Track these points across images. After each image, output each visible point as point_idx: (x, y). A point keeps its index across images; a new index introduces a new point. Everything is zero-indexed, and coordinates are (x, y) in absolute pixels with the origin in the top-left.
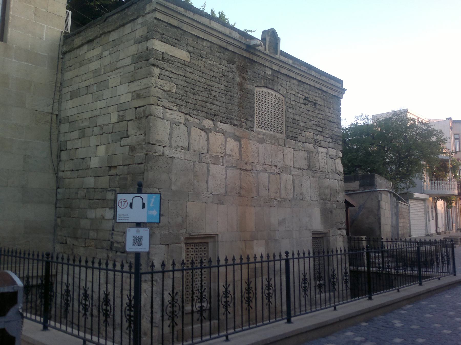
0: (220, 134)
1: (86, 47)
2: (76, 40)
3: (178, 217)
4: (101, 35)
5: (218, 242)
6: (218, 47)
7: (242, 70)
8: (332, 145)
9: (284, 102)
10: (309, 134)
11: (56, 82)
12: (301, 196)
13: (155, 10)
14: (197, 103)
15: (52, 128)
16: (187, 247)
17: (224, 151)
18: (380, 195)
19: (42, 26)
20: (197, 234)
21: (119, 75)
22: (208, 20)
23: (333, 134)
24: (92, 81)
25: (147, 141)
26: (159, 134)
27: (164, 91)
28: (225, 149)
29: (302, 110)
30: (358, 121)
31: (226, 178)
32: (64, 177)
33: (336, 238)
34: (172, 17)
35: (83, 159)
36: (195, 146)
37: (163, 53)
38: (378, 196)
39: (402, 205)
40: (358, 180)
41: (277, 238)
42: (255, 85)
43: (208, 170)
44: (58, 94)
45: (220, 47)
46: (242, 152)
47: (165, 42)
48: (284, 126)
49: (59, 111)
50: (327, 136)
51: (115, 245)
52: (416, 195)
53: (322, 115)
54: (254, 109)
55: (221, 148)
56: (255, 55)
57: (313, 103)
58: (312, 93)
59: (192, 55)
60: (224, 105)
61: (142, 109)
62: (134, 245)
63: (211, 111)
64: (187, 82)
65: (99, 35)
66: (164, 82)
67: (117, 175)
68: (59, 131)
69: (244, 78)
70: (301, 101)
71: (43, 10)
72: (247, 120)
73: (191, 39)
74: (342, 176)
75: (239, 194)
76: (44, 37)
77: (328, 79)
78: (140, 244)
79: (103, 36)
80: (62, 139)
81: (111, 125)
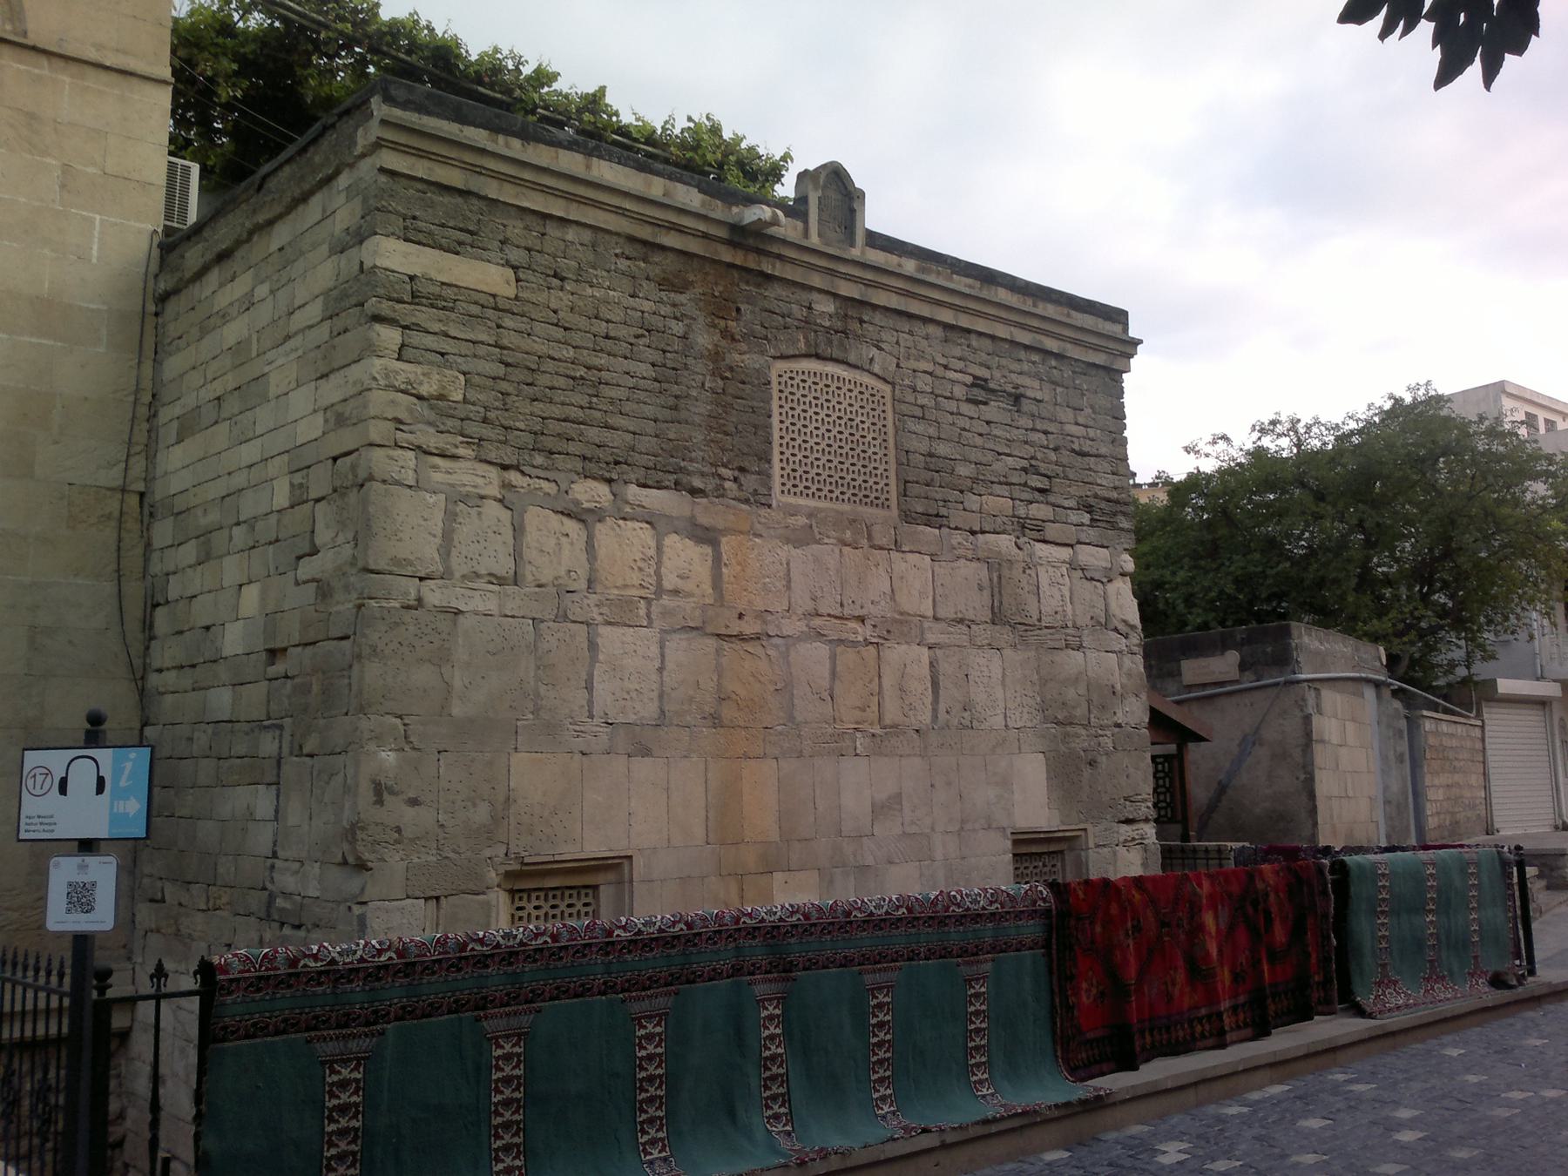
0: (637, 525)
1: (213, 277)
2: (187, 255)
3: (475, 805)
4: (251, 233)
5: (631, 881)
6: (621, 241)
7: (721, 309)
8: (1092, 534)
9: (888, 399)
10: (998, 502)
11: (137, 391)
12: (966, 714)
13: (379, 144)
14: (538, 429)
15: (124, 534)
16: (518, 904)
17: (653, 580)
18: (1311, 697)
19: (85, 219)
20: (550, 858)
21: (293, 356)
22: (579, 157)
23: (1096, 496)
24: (230, 381)
25: (360, 564)
26: (400, 540)
27: (420, 398)
28: (658, 574)
29: (962, 422)
30: (1266, 442)
31: (661, 670)
32: (162, 689)
33: (1115, 853)
34: (444, 161)
35: (207, 628)
36: (542, 567)
37: (412, 278)
38: (1304, 700)
39: (1438, 728)
40: (1236, 646)
41: (870, 861)
42: (772, 352)
43: (593, 646)
44: (145, 426)
45: (632, 239)
46: (725, 578)
47: (419, 243)
48: (893, 481)
49: (149, 479)
50: (1072, 503)
51: (280, 902)
52: (1505, 686)
53: (1046, 433)
54: (770, 434)
55: (640, 569)
56: (769, 254)
57: (1010, 395)
58: (1004, 362)
59: (522, 276)
60: (650, 427)
61: (348, 459)
62: (68, 911)
63: (600, 453)
64: (507, 365)
65: (245, 235)
66: (419, 369)
67: (287, 677)
68: (148, 545)
69: (726, 334)
70: (959, 391)
71: (90, 170)
72: (742, 470)
73: (520, 224)
74: (1136, 639)
75: (715, 720)
76: (95, 253)
77: (1065, 311)
78: (88, 908)
79: (255, 238)
80: (156, 568)
81: (273, 518)
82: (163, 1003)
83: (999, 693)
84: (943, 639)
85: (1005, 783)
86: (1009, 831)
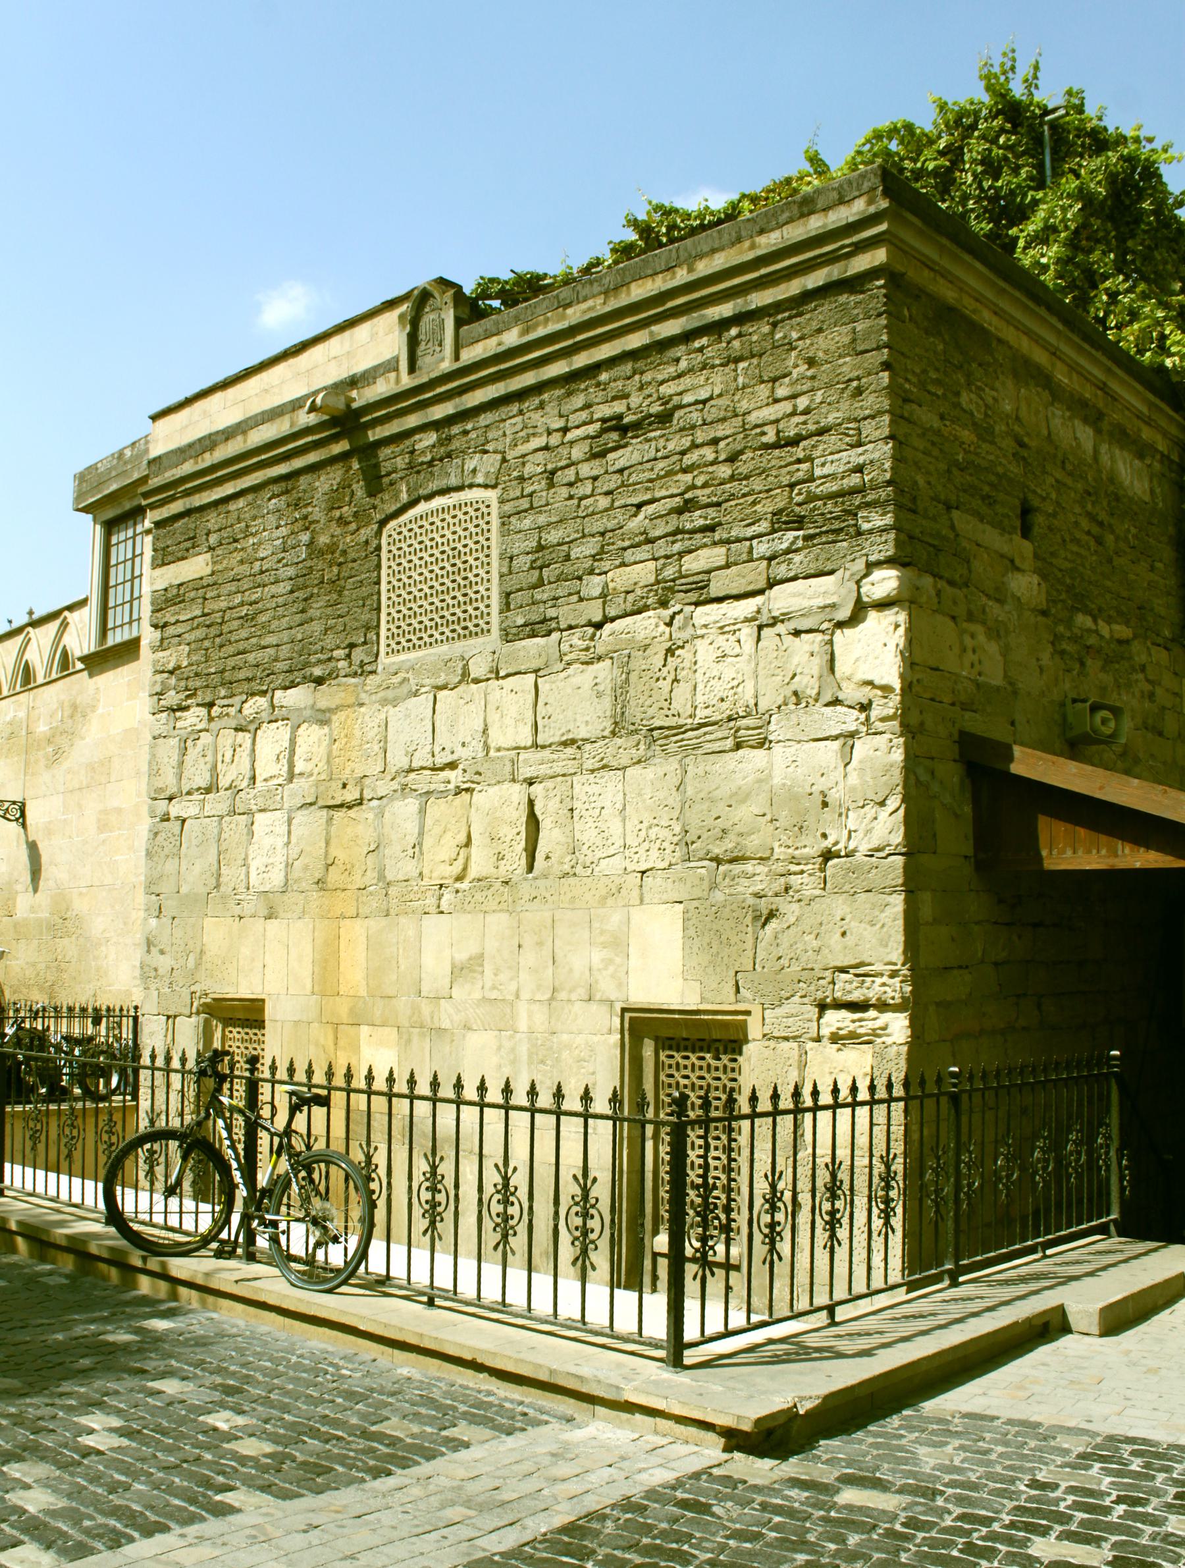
50: (764, 526)
58: (647, 377)
82: (779, 1118)
83: (615, 827)
84: (544, 770)
85: (619, 944)
86: (618, 1007)
